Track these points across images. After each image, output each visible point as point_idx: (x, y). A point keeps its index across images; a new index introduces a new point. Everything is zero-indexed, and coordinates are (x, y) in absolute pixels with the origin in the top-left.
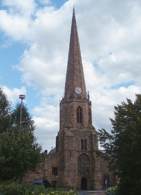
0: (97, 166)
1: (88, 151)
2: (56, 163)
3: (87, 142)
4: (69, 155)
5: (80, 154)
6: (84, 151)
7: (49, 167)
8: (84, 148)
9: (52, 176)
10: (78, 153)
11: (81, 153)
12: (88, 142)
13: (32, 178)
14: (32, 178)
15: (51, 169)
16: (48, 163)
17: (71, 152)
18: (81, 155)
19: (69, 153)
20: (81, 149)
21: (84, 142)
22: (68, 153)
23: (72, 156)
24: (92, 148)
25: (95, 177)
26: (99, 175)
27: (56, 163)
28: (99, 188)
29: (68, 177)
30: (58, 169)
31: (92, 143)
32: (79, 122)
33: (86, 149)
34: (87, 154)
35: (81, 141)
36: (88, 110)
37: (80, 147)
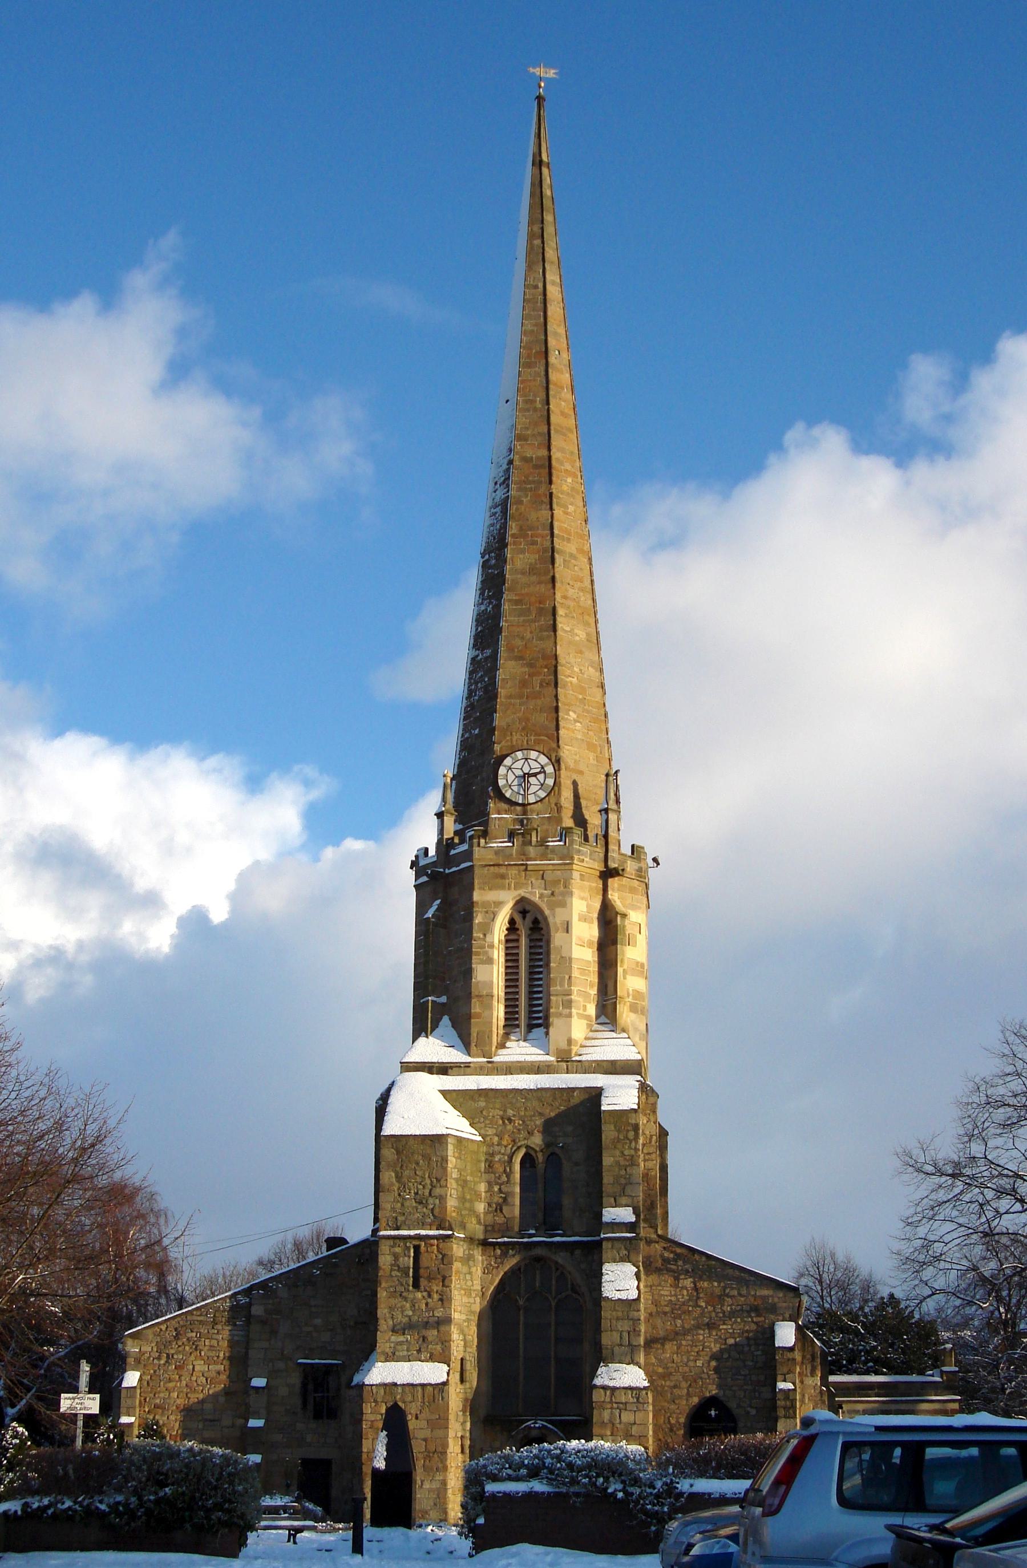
3: (566, 1166)
7: (281, 1365)
9: (300, 1426)
17: (417, 1248)
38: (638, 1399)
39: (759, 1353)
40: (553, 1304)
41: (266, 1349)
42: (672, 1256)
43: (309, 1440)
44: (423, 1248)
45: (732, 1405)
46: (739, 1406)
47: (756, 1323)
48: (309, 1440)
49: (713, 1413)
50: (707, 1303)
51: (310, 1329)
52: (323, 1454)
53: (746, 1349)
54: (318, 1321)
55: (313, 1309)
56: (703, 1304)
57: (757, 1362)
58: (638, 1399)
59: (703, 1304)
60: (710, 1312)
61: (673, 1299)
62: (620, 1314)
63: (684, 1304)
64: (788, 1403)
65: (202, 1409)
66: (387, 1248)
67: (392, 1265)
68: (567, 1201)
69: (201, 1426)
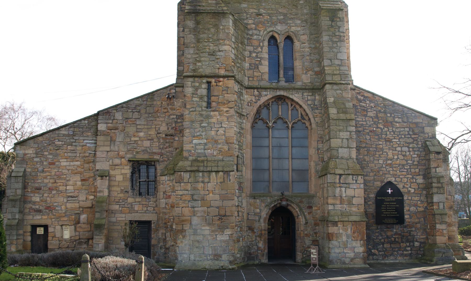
0: (343, 152)
1: (299, 84)
2: (147, 144)
3: (297, 44)
4: (201, 97)
5: (263, 100)
6: (283, 83)
7: (117, 161)
8: (282, 72)
9: (130, 200)
10: (256, 92)
11: (267, 96)
12: (302, 46)
13: (39, 211)
14: (39, 211)
15: (127, 170)
16: (112, 141)
17: (209, 83)
18: (266, 105)
19: (203, 91)
20: (266, 77)
21: (281, 46)
22: (197, 89)
23: (214, 104)
24: (321, 73)
25: (330, 201)
26: (350, 192)
27: (147, 144)
28: (352, 255)
29: (195, 204)
30: (160, 167)
31: (318, 50)
32: (432, 208)
33: (290, 79)
34: (296, 97)
35: (266, 43)
36: (429, 147)
37: (265, 68)
38: (356, 181)
39: (416, 156)
40: (290, 126)
41: (108, 151)
42: (362, 98)
43: (136, 209)
44: (213, 83)
45: (400, 186)
46: (404, 187)
47: (413, 138)
48: (136, 209)
49: (390, 191)
50: (385, 126)
51: (137, 139)
52: (145, 218)
53: (408, 153)
54: (142, 134)
55: (138, 127)
56: (382, 127)
57: (414, 161)
58: (356, 181)
59: (382, 127)
60: (386, 131)
61: (364, 123)
62: (341, 128)
63: (370, 126)
64: (440, 185)
65: (66, 190)
66: (190, 83)
67: (193, 94)
68: (298, 64)
69: (65, 200)
